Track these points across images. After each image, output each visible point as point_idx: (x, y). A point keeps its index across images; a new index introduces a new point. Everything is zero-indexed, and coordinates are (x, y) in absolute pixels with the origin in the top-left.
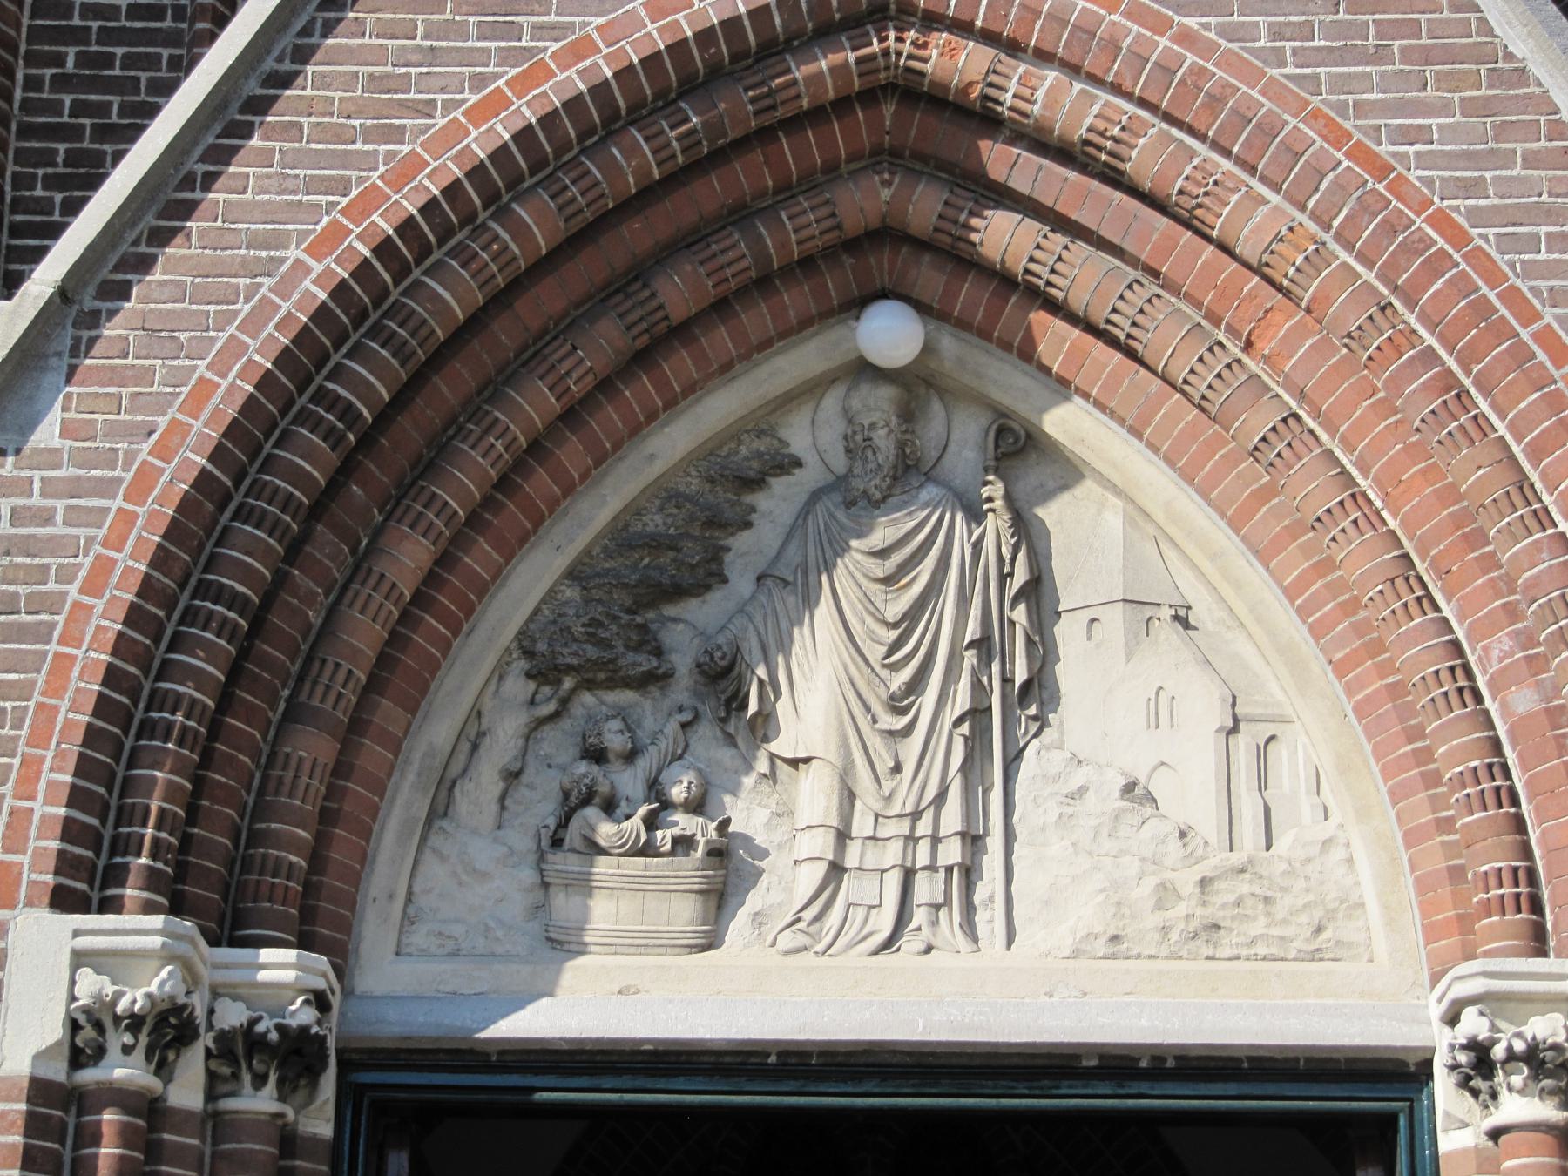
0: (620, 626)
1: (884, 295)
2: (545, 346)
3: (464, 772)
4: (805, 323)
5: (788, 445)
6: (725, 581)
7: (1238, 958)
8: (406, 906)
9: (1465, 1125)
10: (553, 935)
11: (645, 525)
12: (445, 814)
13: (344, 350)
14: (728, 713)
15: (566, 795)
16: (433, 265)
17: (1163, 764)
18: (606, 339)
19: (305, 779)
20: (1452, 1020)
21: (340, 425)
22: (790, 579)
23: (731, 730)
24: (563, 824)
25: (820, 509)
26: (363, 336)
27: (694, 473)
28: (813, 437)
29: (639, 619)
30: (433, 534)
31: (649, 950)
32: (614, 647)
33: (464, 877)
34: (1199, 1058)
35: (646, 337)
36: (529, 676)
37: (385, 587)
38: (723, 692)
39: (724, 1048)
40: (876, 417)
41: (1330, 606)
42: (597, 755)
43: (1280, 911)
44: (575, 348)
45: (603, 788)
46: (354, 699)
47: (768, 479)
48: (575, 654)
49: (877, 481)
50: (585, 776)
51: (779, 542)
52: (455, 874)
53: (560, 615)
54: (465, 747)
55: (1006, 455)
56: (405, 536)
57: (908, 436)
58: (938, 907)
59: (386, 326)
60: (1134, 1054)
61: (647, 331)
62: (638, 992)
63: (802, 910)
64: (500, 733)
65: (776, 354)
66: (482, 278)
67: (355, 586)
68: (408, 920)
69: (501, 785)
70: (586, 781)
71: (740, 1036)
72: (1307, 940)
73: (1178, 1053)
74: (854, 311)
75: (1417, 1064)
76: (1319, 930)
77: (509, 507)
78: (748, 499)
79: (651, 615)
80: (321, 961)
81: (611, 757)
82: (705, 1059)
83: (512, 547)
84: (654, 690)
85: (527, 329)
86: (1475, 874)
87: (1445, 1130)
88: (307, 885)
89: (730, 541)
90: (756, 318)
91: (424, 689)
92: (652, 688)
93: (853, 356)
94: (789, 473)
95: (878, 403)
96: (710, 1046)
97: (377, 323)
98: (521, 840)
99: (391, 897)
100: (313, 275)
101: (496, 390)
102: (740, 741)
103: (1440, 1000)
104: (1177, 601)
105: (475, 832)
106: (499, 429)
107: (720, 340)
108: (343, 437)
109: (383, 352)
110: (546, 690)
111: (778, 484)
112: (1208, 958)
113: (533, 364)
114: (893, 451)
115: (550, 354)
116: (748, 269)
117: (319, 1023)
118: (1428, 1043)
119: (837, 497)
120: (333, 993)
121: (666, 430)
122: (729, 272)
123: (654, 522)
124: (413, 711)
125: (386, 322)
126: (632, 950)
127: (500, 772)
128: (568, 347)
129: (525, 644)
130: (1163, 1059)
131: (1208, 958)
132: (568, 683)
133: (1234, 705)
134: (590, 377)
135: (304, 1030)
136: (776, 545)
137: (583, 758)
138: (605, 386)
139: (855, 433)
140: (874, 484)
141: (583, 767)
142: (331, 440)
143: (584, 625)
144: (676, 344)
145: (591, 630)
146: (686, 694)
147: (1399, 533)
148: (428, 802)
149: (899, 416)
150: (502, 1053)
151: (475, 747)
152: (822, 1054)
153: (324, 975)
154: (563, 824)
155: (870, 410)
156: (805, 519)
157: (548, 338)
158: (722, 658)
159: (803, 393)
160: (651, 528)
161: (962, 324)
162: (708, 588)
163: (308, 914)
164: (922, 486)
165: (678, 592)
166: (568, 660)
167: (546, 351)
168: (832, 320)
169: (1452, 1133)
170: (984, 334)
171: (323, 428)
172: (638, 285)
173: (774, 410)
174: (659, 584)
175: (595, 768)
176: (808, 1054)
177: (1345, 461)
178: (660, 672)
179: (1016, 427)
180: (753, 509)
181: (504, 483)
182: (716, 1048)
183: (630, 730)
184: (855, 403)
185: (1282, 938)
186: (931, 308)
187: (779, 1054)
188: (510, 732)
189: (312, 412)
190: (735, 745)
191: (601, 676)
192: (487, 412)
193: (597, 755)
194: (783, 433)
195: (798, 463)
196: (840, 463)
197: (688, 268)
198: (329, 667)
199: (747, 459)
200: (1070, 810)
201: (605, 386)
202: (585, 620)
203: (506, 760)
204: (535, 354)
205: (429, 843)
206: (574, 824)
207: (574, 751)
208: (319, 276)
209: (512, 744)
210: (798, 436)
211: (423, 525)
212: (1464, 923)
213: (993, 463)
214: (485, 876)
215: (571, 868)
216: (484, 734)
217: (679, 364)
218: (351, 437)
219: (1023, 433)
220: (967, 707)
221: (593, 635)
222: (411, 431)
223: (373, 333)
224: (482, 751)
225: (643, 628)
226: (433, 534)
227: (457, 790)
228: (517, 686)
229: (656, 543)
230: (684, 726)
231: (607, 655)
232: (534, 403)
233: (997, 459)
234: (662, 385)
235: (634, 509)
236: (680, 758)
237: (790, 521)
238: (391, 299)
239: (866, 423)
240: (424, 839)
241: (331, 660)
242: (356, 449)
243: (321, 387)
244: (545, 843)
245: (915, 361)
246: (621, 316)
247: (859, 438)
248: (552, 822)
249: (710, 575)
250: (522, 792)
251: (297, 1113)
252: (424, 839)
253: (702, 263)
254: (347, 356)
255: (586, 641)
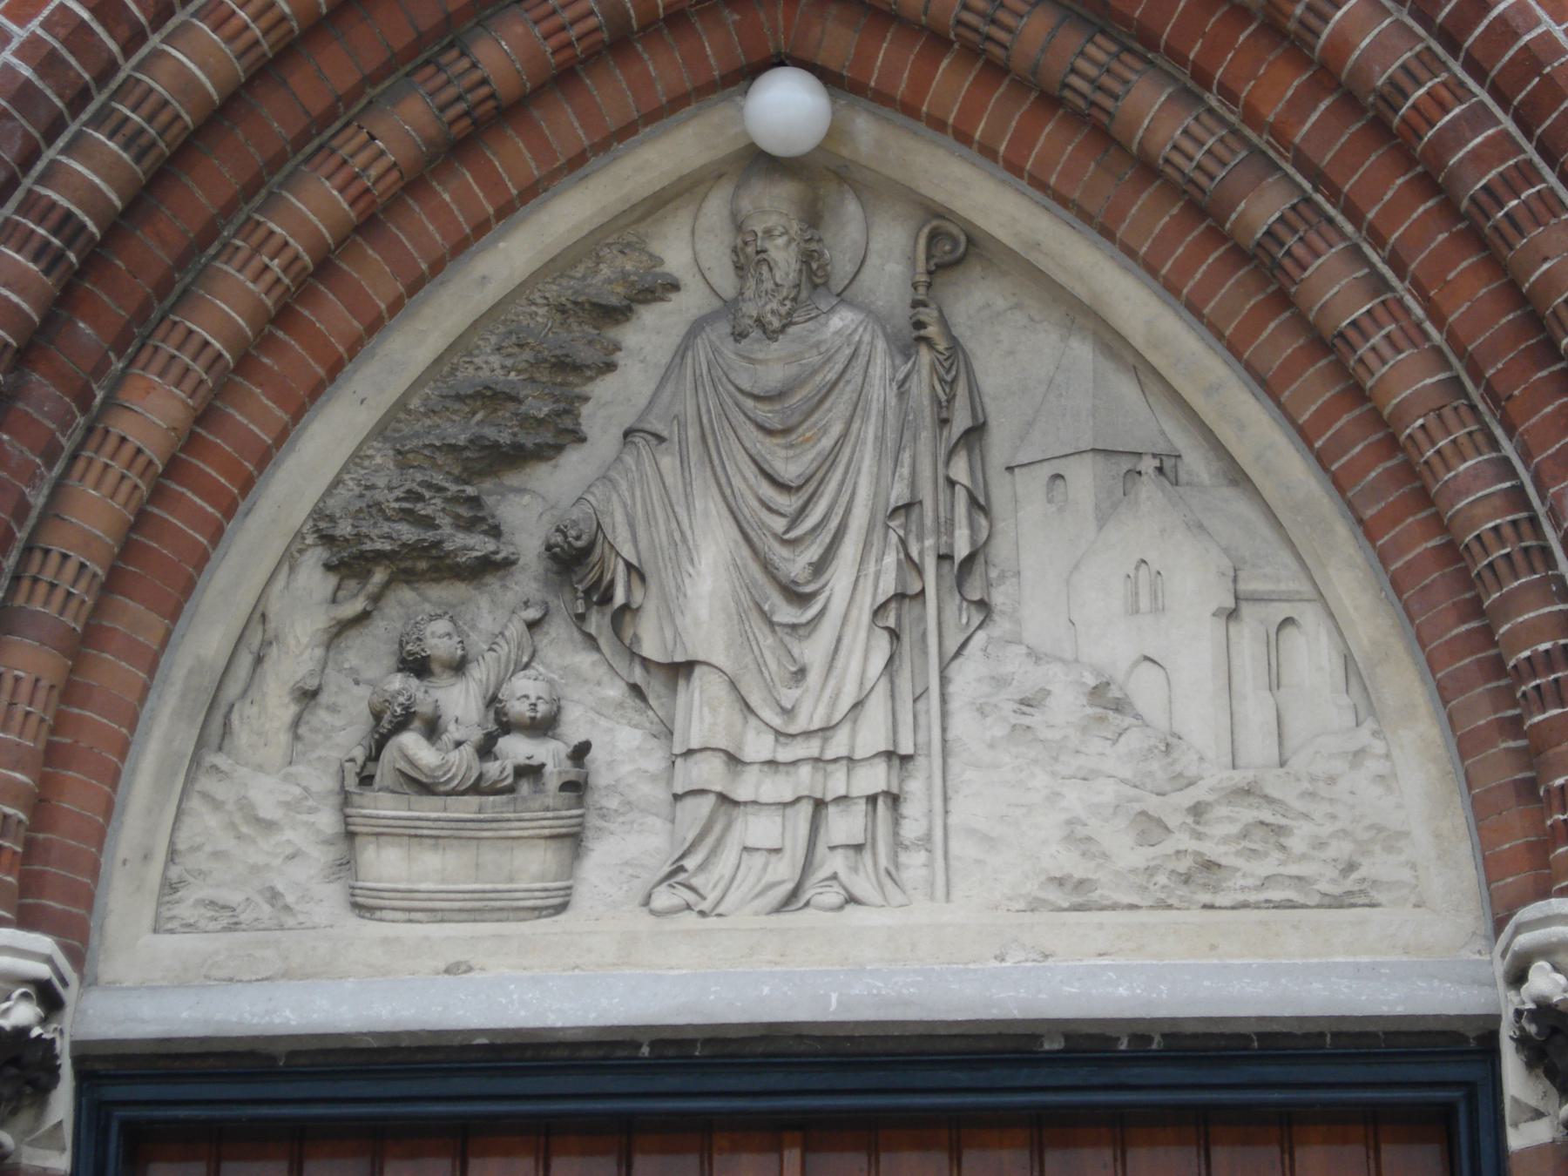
0: (447, 500)
1: (779, 61)
2: (334, 136)
3: (245, 693)
4: (678, 103)
5: (661, 262)
6: (583, 440)
7: (1244, 905)
8: (166, 868)
9: (1538, 1115)
10: (359, 899)
11: (478, 368)
12: (220, 749)
13: (60, 143)
14: (588, 606)
15: (377, 716)
16: (177, 28)
17: (1147, 658)
18: (406, 122)
19: (22, 707)
20: (1518, 978)
21: (56, 242)
22: (665, 434)
23: (593, 631)
24: (374, 756)
25: (701, 343)
26: (86, 124)
27: (540, 301)
28: (689, 250)
29: (470, 490)
30: (189, 383)
31: (487, 916)
32: (437, 527)
33: (244, 829)
34: (1195, 1036)
35: (466, 122)
36: (328, 567)
37: (127, 452)
38: (580, 581)
39: (580, 1038)
40: (773, 221)
41: (1358, 449)
42: (418, 666)
43: (1296, 844)
44: (373, 138)
45: (424, 708)
46: (89, 601)
47: (636, 307)
48: (389, 537)
49: (774, 305)
50: (399, 693)
51: (653, 386)
52: (232, 826)
53: (367, 488)
54: (245, 660)
55: (943, 267)
56: (151, 387)
57: (814, 246)
58: (858, 848)
59: (114, 110)
60: (1111, 1032)
61: (467, 114)
62: (470, 969)
63: (682, 857)
64: (292, 642)
65: (642, 143)
66: (241, 43)
67: (87, 453)
68: (170, 887)
69: (293, 709)
70: (401, 699)
71: (602, 1022)
72: (1333, 881)
73: (1166, 1030)
74: (743, 84)
75: (1479, 1038)
76: (1351, 867)
77: (295, 346)
78: (613, 333)
79: (488, 484)
80: (43, 942)
81: (436, 668)
82: (558, 1053)
83: (302, 403)
84: (493, 582)
85: (307, 113)
86: (1548, 791)
87: (1515, 1125)
88: (29, 844)
89: (587, 389)
90: (611, 93)
91: (189, 587)
92: (489, 579)
93: (742, 143)
94: (662, 299)
95: (773, 206)
96: (560, 1036)
97: (104, 106)
98: (323, 782)
99: (147, 857)
100: (14, 44)
101: (271, 193)
102: (602, 642)
103: (1503, 955)
104: (1161, 448)
105: (260, 768)
106: (274, 243)
107: (564, 124)
108: (60, 256)
109: (111, 144)
110: (352, 584)
111: (649, 315)
112: (1205, 907)
113: (318, 159)
114: (795, 266)
115: (341, 147)
116: (596, 29)
117: (43, 1022)
118: (1492, 1011)
119: (724, 328)
120: (65, 983)
121: (502, 245)
122: (573, 33)
123: (490, 366)
124: (174, 615)
125: (114, 105)
126: (464, 916)
127: (293, 690)
128: (364, 136)
129: (322, 525)
130: (1148, 1039)
131: (1205, 907)
132: (379, 576)
133: (1235, 580)
134: (395, 174)
135: (21, 1032)
136: (647, 391)
137: (399, 670)
138: (415, 182)
139: (746, 243)
140: (771, 308)
141: (397, 682)
142: (44, 262)
143: (398, 500)
144: (510, 132)
145: (406, 505)
146: (534, 585)
147: (1446, 348)
148: (195, 732)
149: (801, 220)
150: (292, 1054)
151: (259, 660)
152: (708, 1042)
153: (49, 960)
154: (374, 756)
155: (763, 212)
156: (683, 358)
157: (338, 125)
158: (578, 538)
159: (679, 195)
160: (485, 374)
161: (882, 98)
162: (559, 448)
163: (30, 883)
164: (832, 310)
165: (515, 457)
166: (378, 546)
167: (334, 143)
168: (714, 97)
169: (1523, 1126)
170: (910, 110)
171: (34, 245)
172: (454, 53)
173: (642, 219)
174: (496, 445)
175: (414, 682)
176: (692, 1042)
177: (1375, 258)
178: (499, 557)
179: (954, 230)
180: (617, 348)
181: (284, 315)
182: (569, 1037)
183: (460, 632)
184: (746, 205)
185: (1300, 878)
186: (841, 76)
187: (653, 1044)
188: (304, 640)
189: (18, 223)
190: (598, 649)
191: (422, 565)
192: (258, 223)
193: (418, 666)
194: (656, 247)
195: (674, 286)
196: (726, 282)
197: (519, 29)
198: (54, 559)
199: (609, 281)
200: (1026, 720)
201: (415, 182)
202: (399, 493)
203: (299, 676)
204: (321, 147)
205: (198, 787)
206: (389, 753)
207: (391, 661)
208: (23, 45)
209: (306, 656)
210: (674, 250)
211: (175, 371)
212: (1540, 850)
213: (924, 278)
214: (269, 826)
215: (382, 813)
216: (270, 643)
217: (512, 157)
218: (72, 256)
219: (963, 239)
220: (892, 593)
221: (410, 512)
222: (153, 246)
223: (96, 122)
224: (267, 665)
225: (475, 502)
226: (189, 383)
227: (235, 717)
228: (312, 578)
229: (492, 397)
230: (532, 625)
231: (430, 535)
232: (313, 206)
233: (930, 273)
234: (492, 183)
235: (460, 346)
236: (527, 666)
237: (665, 360)
238: (121, 76)
239: (759, 229)
240: (190, 779)
241: (57, 549)
242: (80, 273)
243: (30, 191)
244: (352, 783)
245: (820, 148)
246: (431, 94)
247: (750, 250)
248: (359, 754)
249: (563, 433)
250: (321, 717)
251: (19, 1141)
252: (190, 779)
253: (536, 22)
254: (63, 151)
255: (401, 520)
